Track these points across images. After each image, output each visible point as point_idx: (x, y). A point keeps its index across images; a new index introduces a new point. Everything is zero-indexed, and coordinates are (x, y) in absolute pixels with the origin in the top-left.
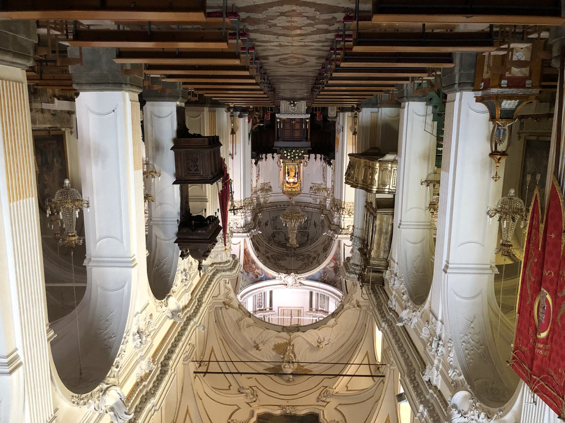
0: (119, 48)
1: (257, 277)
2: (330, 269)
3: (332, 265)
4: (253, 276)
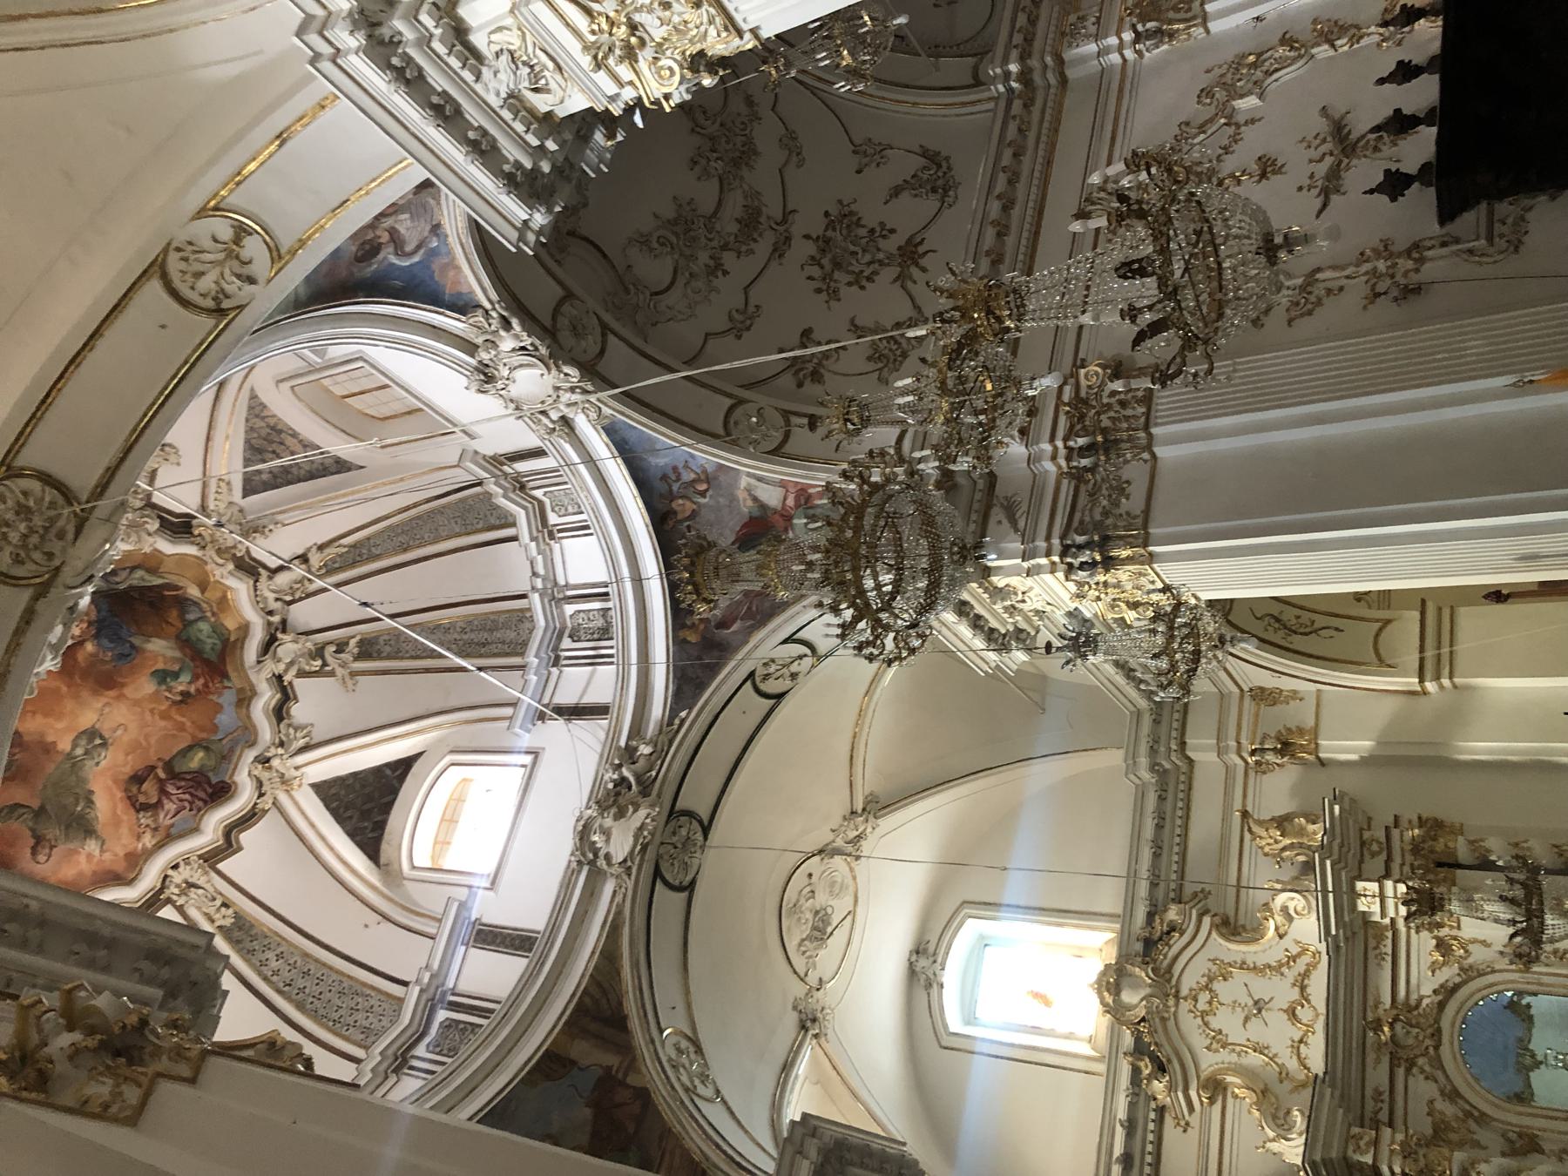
2: (741, 495)
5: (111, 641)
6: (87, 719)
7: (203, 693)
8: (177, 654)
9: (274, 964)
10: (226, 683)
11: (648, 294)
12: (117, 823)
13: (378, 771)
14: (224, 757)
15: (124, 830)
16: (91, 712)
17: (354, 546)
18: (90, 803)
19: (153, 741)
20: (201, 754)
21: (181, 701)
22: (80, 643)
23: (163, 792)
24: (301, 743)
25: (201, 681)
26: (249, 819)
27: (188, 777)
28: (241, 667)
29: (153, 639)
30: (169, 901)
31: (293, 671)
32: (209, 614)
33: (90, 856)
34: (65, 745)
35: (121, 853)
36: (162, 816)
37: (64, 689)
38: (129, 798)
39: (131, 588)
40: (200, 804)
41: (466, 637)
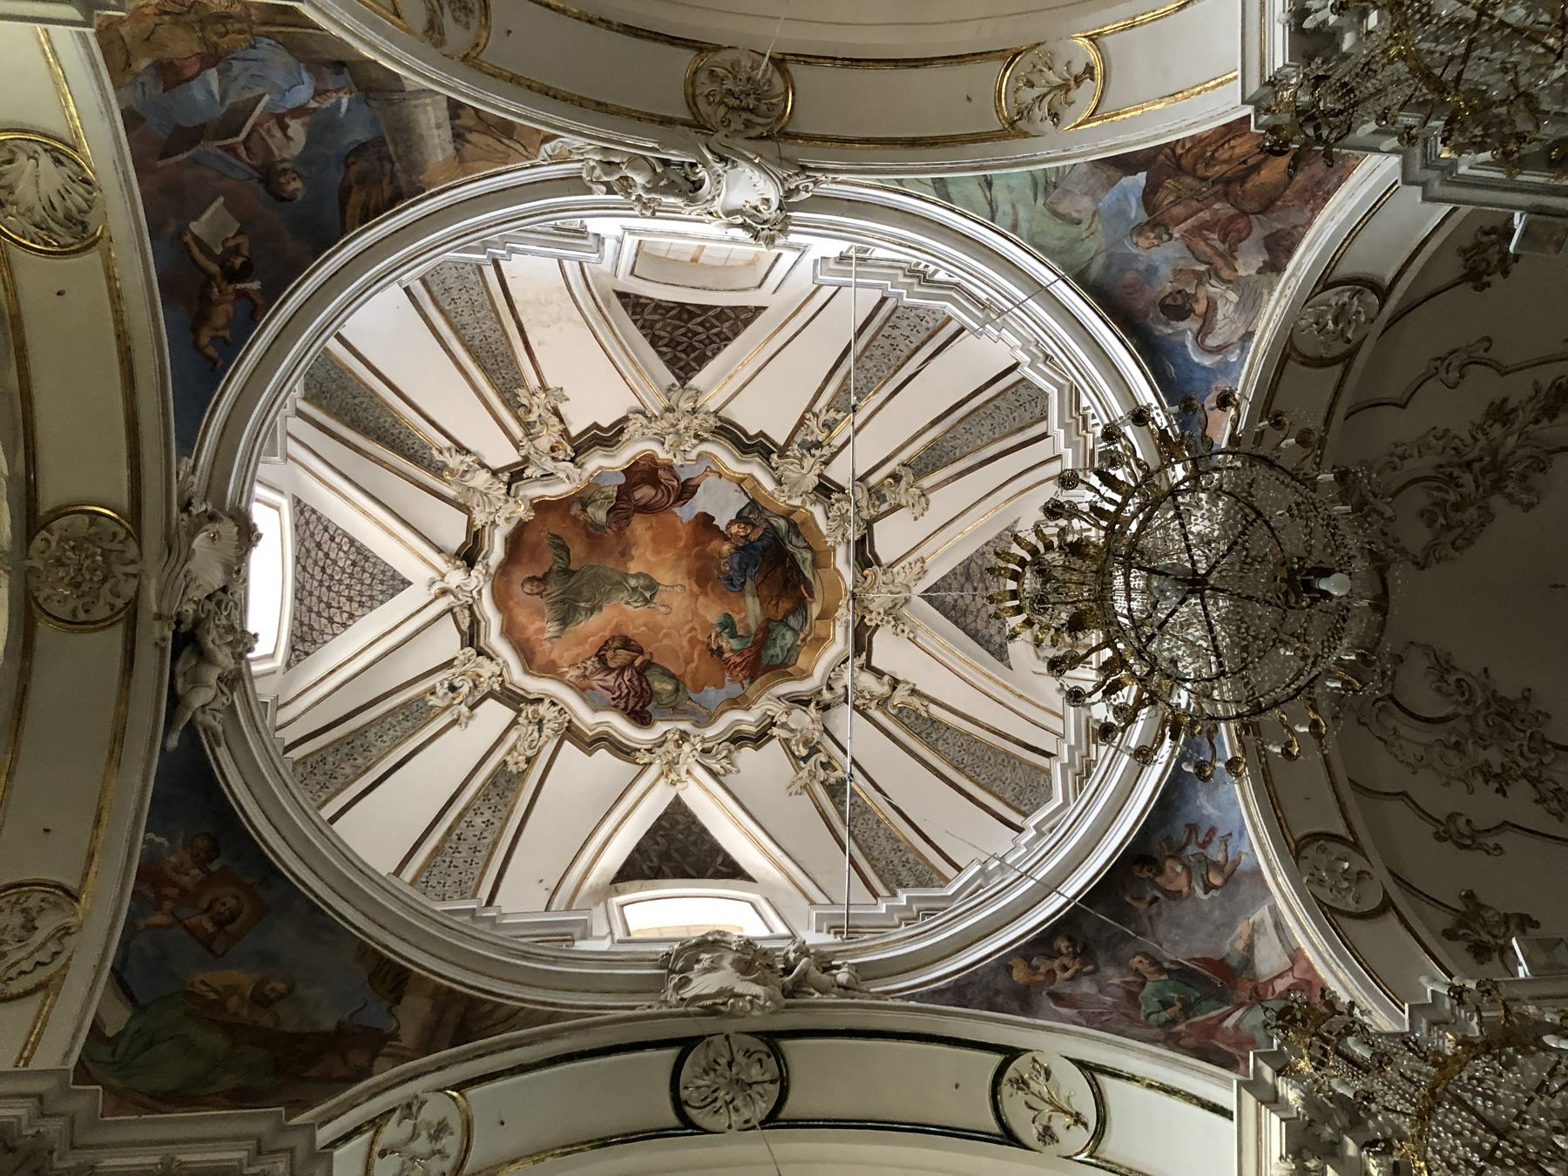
0: (688, 927)
1: (1177, 309)
2: (1242, 929)
3: (1269, 959)
4: (1165, 271)
5: (739, 563)
6: (664, 577)
7: (727, 665)
8: (754, 628)
9: (478, 820)
10: (746, 682)
11: (1388, 691)
12: (581, 642)
13: (716, 849)
14: (674, 708)
15: (575, 651)
16: (671, 577)
17: (934, 721)
18: (592, 611)
19: (666, 642)
20: (669, 687)
21: (712, 650)
22: (725, 538)
23: (622, 670)
24: (716, 767)
25: (738, 660)
26: (623, 751)
27: (644, 685)
28: (765, 687)
29: (757, 599)
30: (519, 712)
31: (784, 734)
32: (802, 636)
33: (542, 630)
34: (633, 568)
35: (554, 655)
36: (599, 677)
37: (681, 544)
38: (607, 642)
39: (792, 556)
40: (622, 705)
41: (900, 868)
